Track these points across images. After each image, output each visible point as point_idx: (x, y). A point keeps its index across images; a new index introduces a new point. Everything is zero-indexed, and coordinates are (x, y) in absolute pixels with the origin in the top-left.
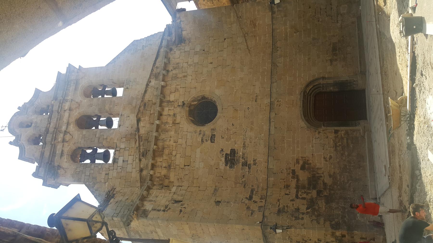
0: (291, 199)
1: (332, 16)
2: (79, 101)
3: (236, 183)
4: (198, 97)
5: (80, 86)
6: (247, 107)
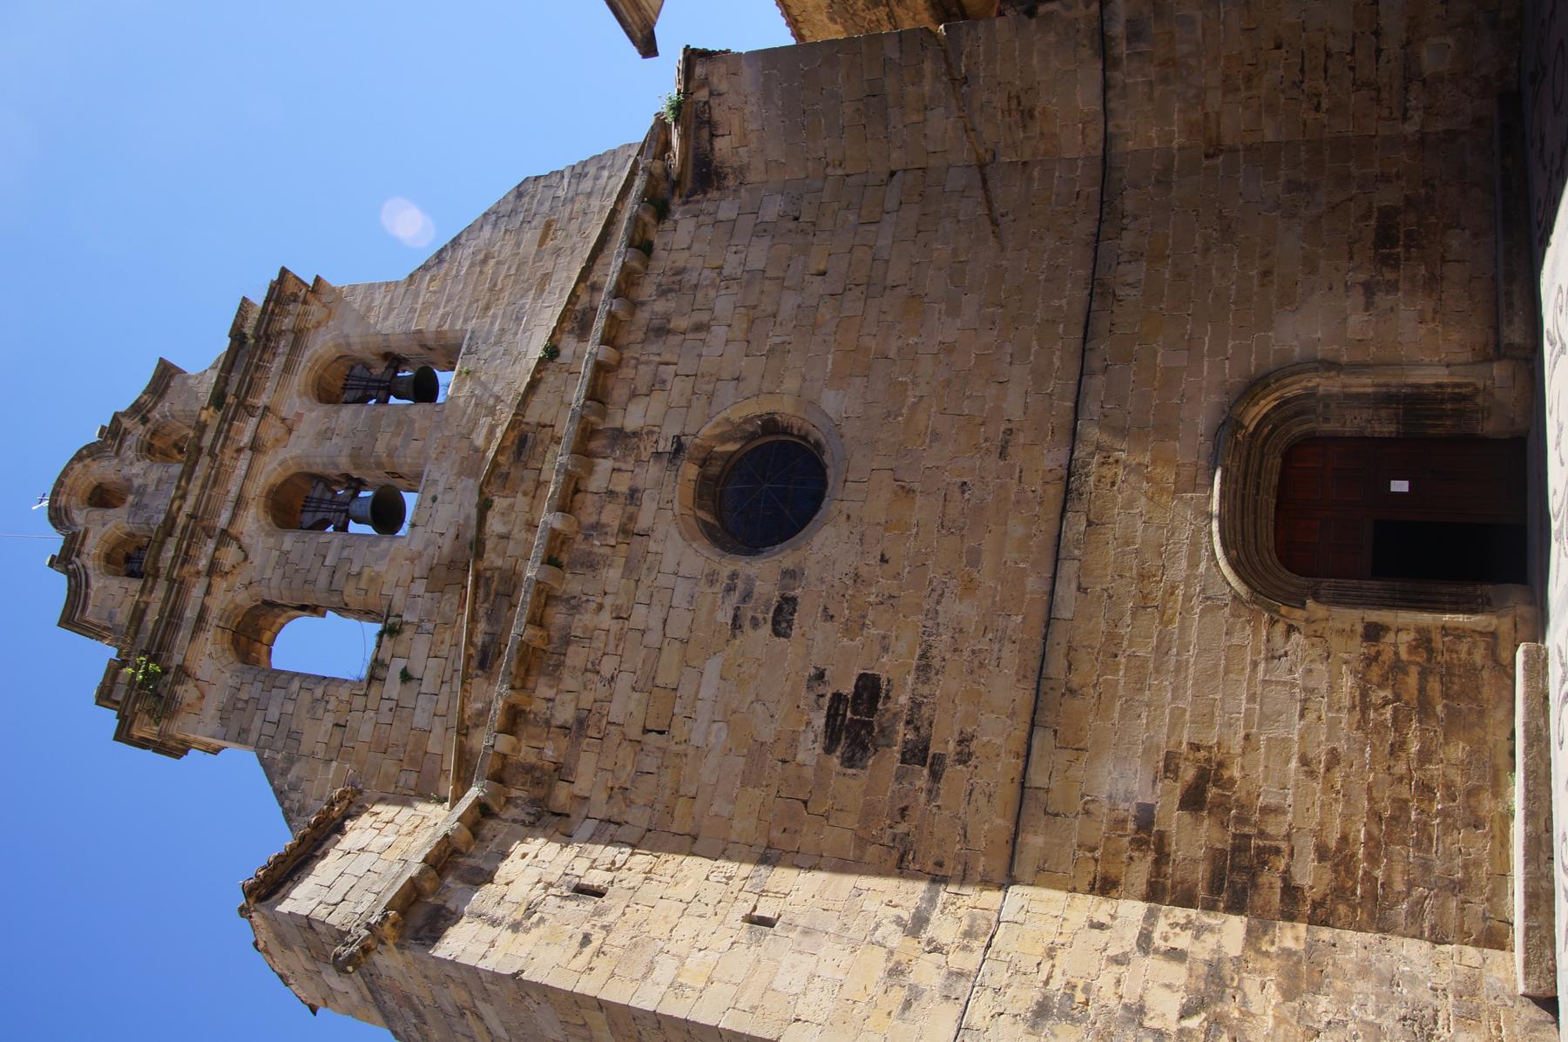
0: (1112, 952)
1: (1379, 90)
2: (291, 416)
4: (747, 420)
5: (308, 353)
6: (959, 480)
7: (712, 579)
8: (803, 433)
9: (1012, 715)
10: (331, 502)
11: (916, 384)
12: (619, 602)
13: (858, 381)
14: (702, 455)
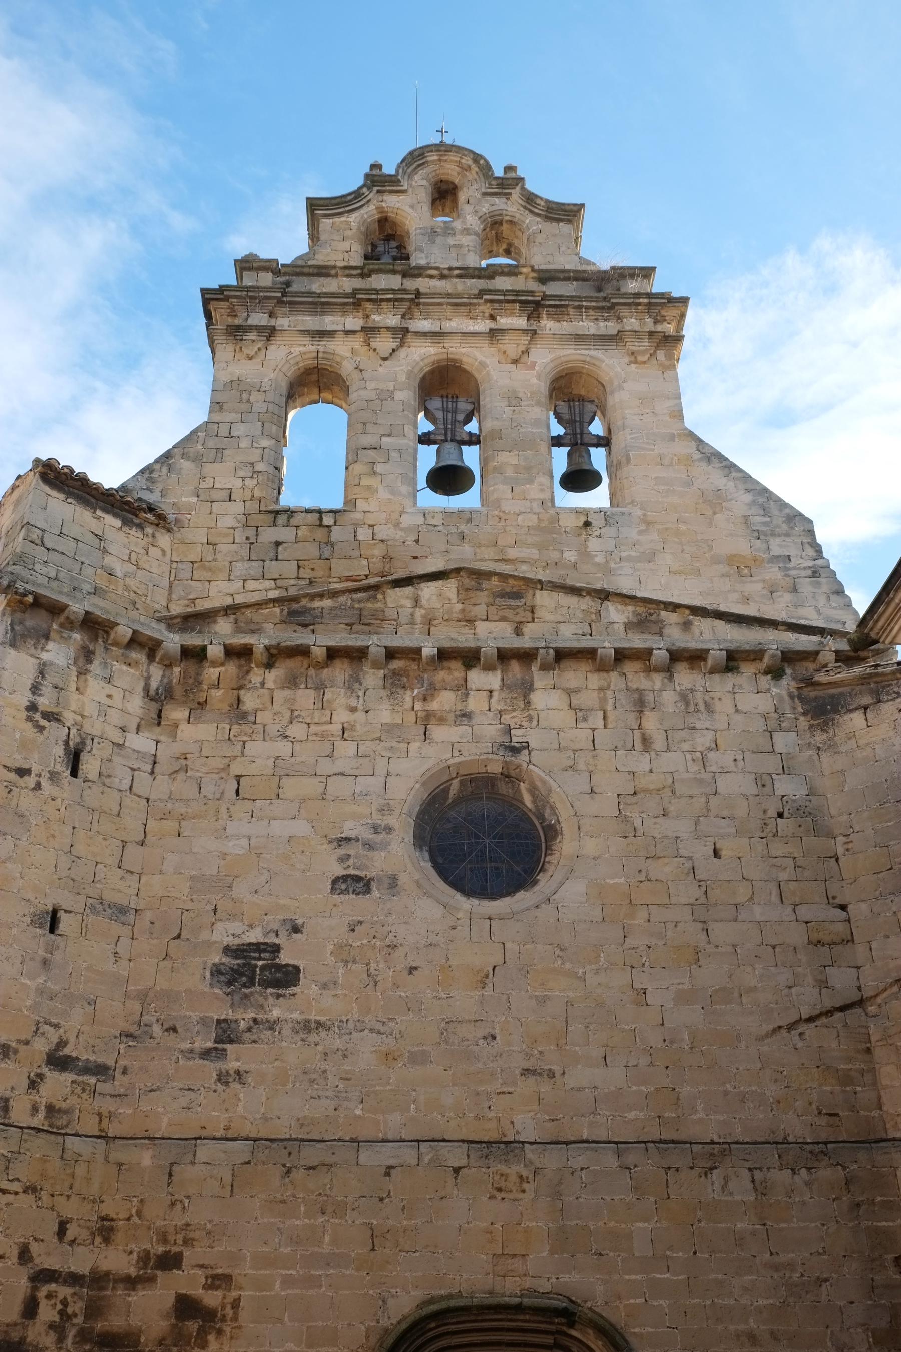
0: (34, 1248)
3: (143, 997)
4: (553, 809)
5: (598, 354)
6: (497, 1032)
7: (385, 809)
8: (547, 866)
9: (266, 1119)
10: (455, 421)
11: (597, 972)
12: (358, 727)
13: (598, 913)
14: (513, 773)
